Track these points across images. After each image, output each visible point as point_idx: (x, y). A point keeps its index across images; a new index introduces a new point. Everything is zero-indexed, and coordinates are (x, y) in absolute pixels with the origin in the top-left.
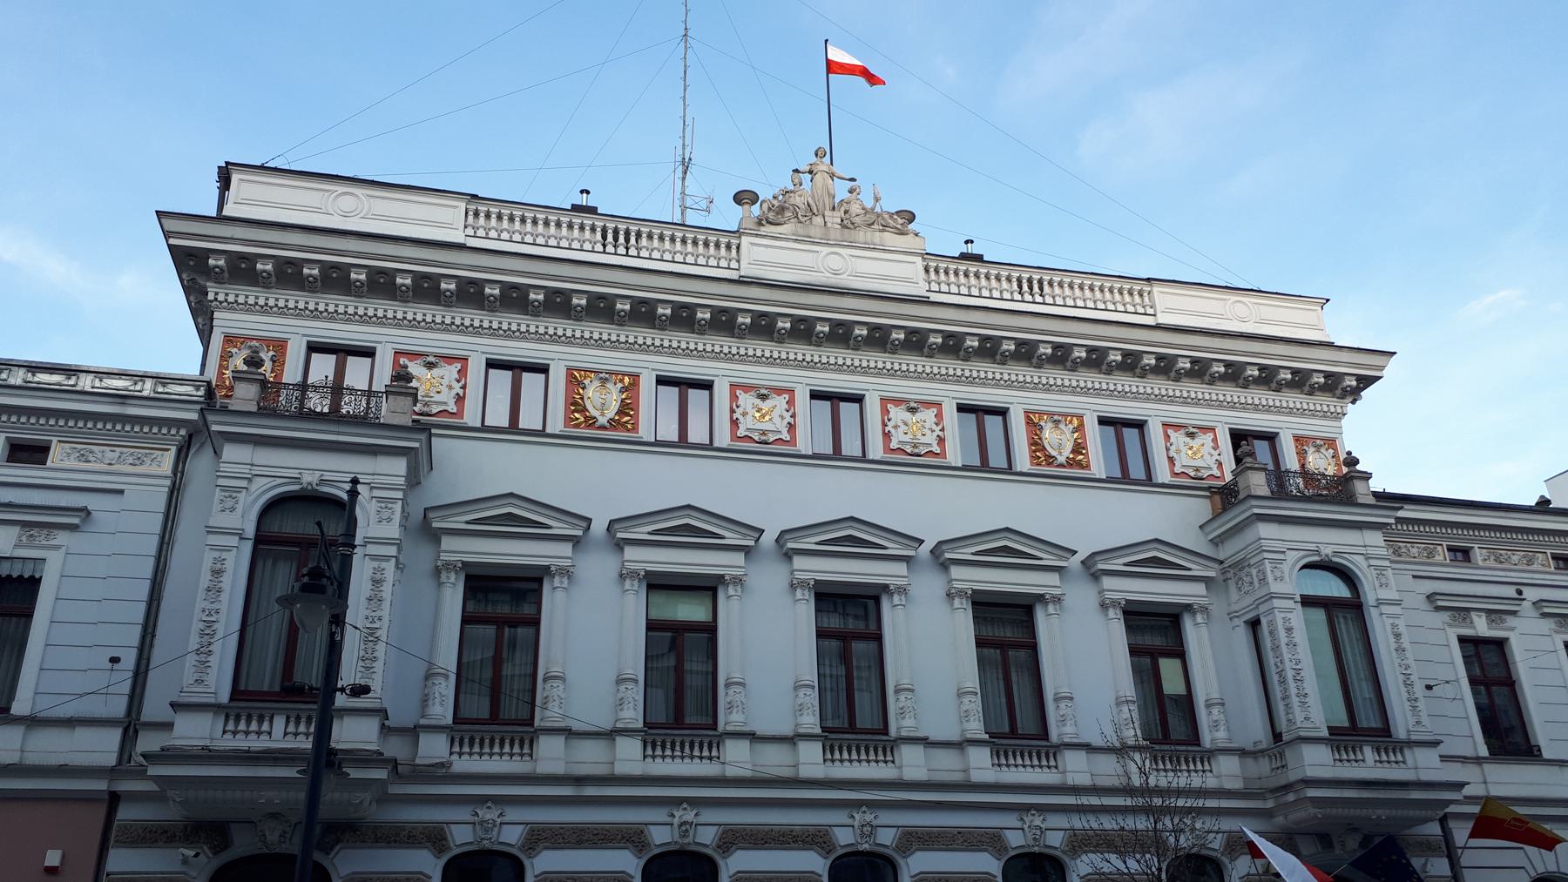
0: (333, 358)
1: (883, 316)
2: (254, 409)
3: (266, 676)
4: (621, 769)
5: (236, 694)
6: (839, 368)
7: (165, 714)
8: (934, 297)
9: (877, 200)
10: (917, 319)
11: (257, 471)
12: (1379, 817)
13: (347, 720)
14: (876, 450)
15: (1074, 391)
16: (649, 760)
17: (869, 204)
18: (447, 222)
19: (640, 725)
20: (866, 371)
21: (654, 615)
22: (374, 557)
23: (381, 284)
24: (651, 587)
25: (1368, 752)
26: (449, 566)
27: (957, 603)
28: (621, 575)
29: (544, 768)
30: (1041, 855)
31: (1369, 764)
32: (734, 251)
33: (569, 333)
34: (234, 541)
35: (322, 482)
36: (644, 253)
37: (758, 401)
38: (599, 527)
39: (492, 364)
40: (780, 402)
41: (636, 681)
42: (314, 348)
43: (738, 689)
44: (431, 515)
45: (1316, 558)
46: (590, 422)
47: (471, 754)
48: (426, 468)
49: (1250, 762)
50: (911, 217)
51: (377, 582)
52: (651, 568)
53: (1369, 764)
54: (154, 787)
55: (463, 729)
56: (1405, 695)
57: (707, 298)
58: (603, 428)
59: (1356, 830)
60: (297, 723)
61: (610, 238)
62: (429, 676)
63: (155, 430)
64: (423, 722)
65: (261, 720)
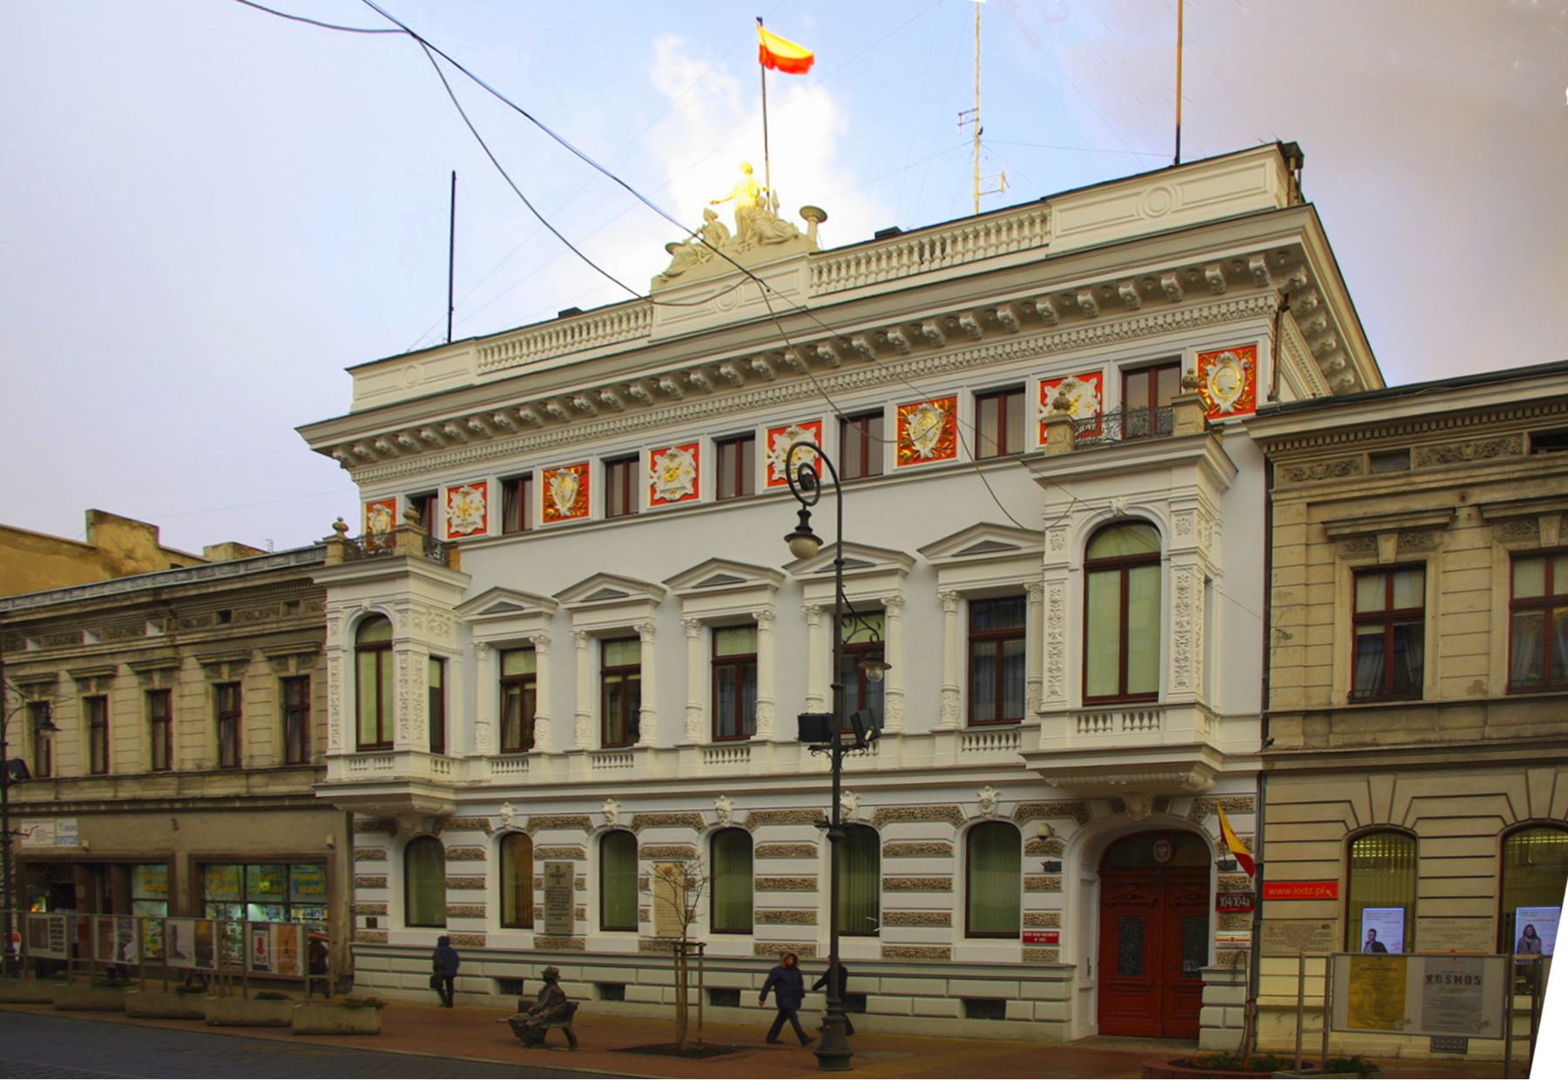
0: (1146, 375)
2: (1069, 450)
3: (1105, 685)
5: (1087, 700)
6: (730, 410)
7: (1037, 720)
12: (1118, 783)
13: (1171, 714)
15: (944, 369)
18: (467, 369)
20: (752, 406)
21: (609, 663)
22: (1180, 568)
30: (730, 829)
31: (1118, 733)
34: (1065, 573)
40: (686, 458)
41: (957, 692)
46: (917, 458)
50: (822, 217)
53: (1118, 733)
54: (1037, 776)
58: (566, 517)
60: (1132, 720)
63: (1304, 444)
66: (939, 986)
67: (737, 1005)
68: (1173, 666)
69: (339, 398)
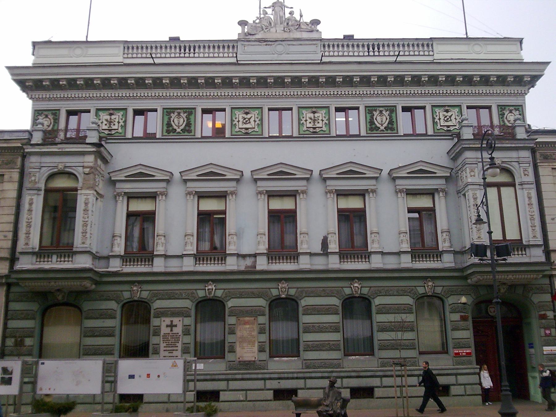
1: (104, 73)
4: (185, 269)
8: (325, 59)
9: (301, 16)
10: (123, 72)
11: (43, 165)
14: (430, 132)
16: (342, 263)
17: (298, 18)
19: (338, 251)
23: (89, 84)
24: (338, 195)
25: (54, 257)
26: (119, 194)
27: (399, 195)
28: (396, 192)
29: (155, 269)
32: (430, 47)
33: (146, 95)
35: (65, 167)
36: (381, 54)
37: (445, 113)
38: (316, 174)
39: (270, 109)
41: (265, 235)
42: (70, 113)
43: (189, 237)
44: (322, 172)
45: (56, 170)
47: (218, 264)
48: (109, 157)
49: (241, 260)
51: (86, 204)
52: (127, 191)
55: (127, 258)
56: (530, 224)
57: (424, 71)
59: (504, 284)
61: (371, 49)
62: (114, 236)
64: (111, 254)
65: (48, 257)
66: (259, 384)
67: (373, 397)
68: (80, 235)
69: (27, 59)
